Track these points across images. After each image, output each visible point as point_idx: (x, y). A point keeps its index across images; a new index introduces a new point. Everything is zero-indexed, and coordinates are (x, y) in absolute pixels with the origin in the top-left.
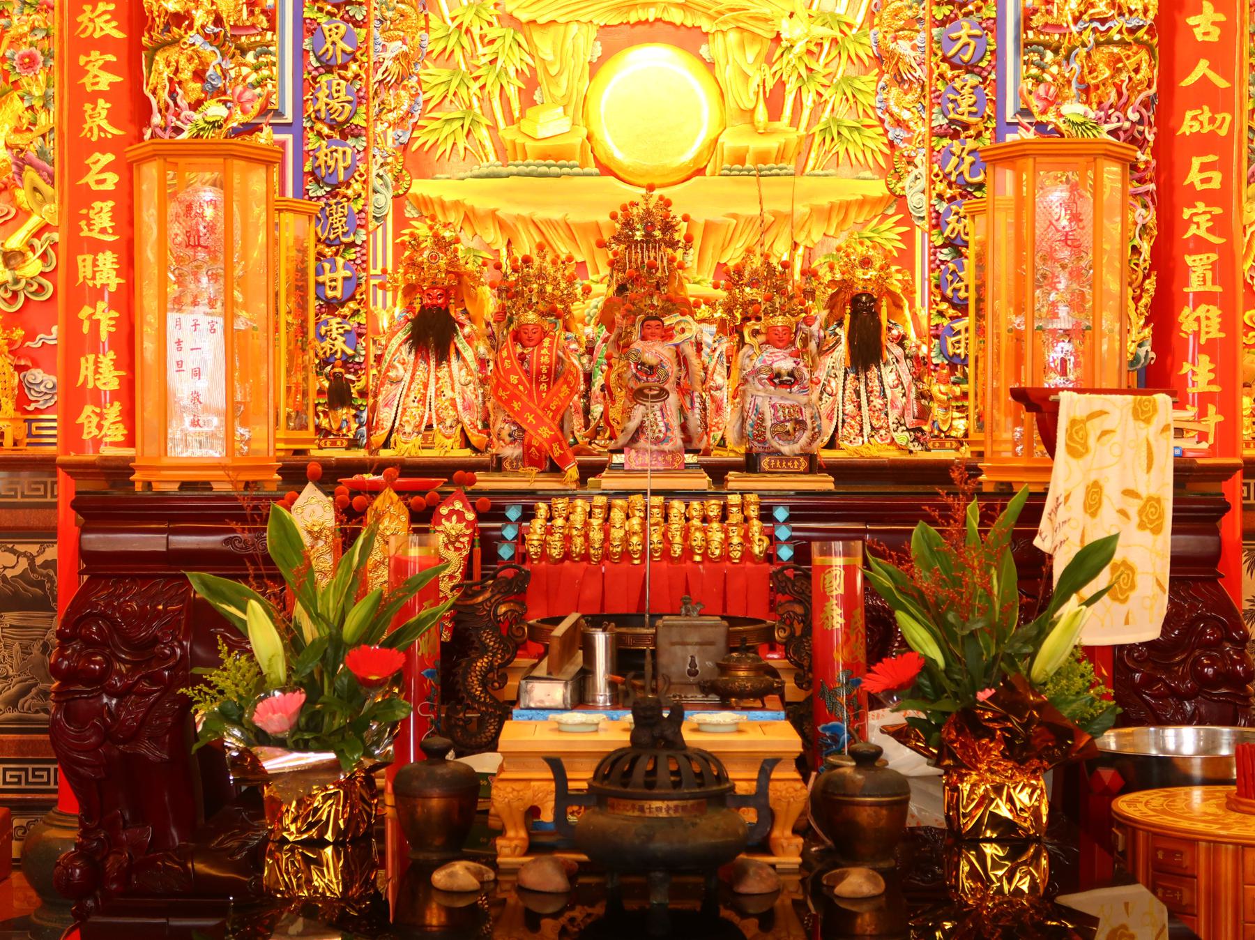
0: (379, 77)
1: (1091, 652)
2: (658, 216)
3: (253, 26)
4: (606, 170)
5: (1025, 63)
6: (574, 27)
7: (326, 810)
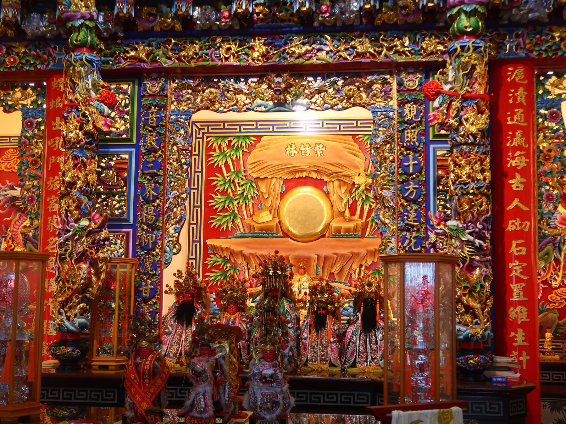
0: (167, 205)
2: (279, 263)
3: (118, 185)
4: (286, 235)
5: (438, 199)
6: (274, 180)
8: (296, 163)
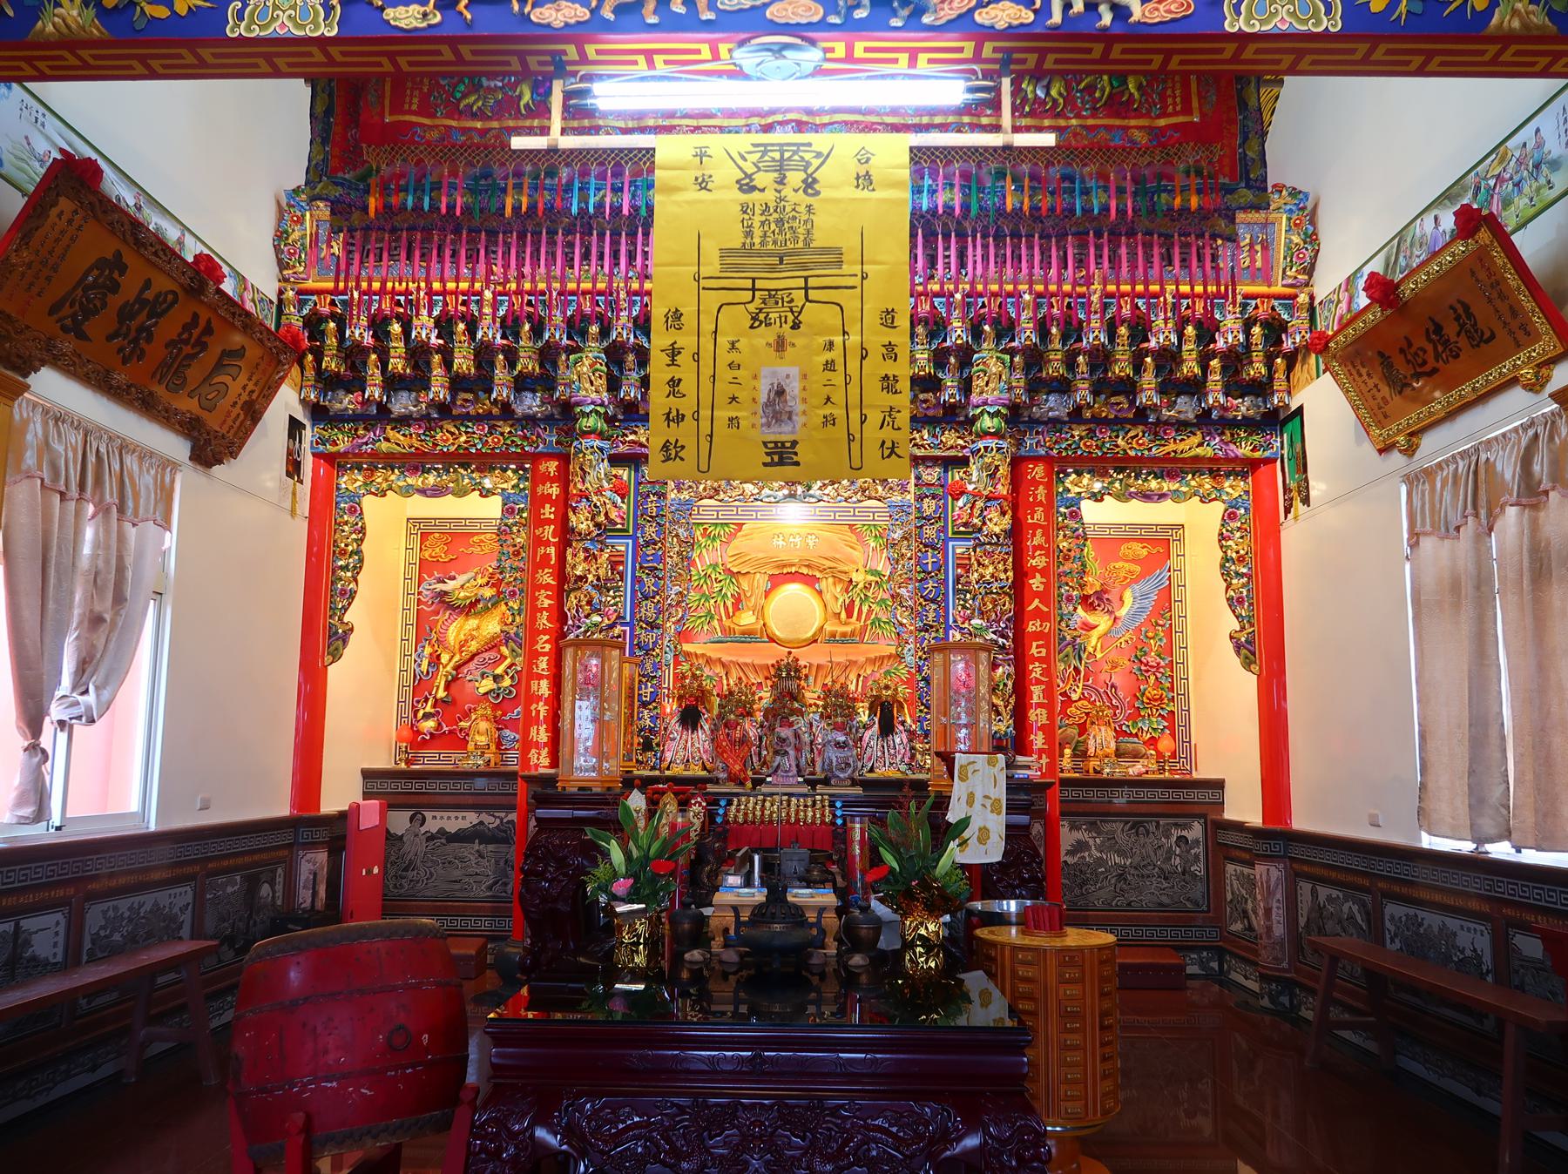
1: (964, 867)
4: (772, 640)
7: (641, 929)
8: (784, 557)
